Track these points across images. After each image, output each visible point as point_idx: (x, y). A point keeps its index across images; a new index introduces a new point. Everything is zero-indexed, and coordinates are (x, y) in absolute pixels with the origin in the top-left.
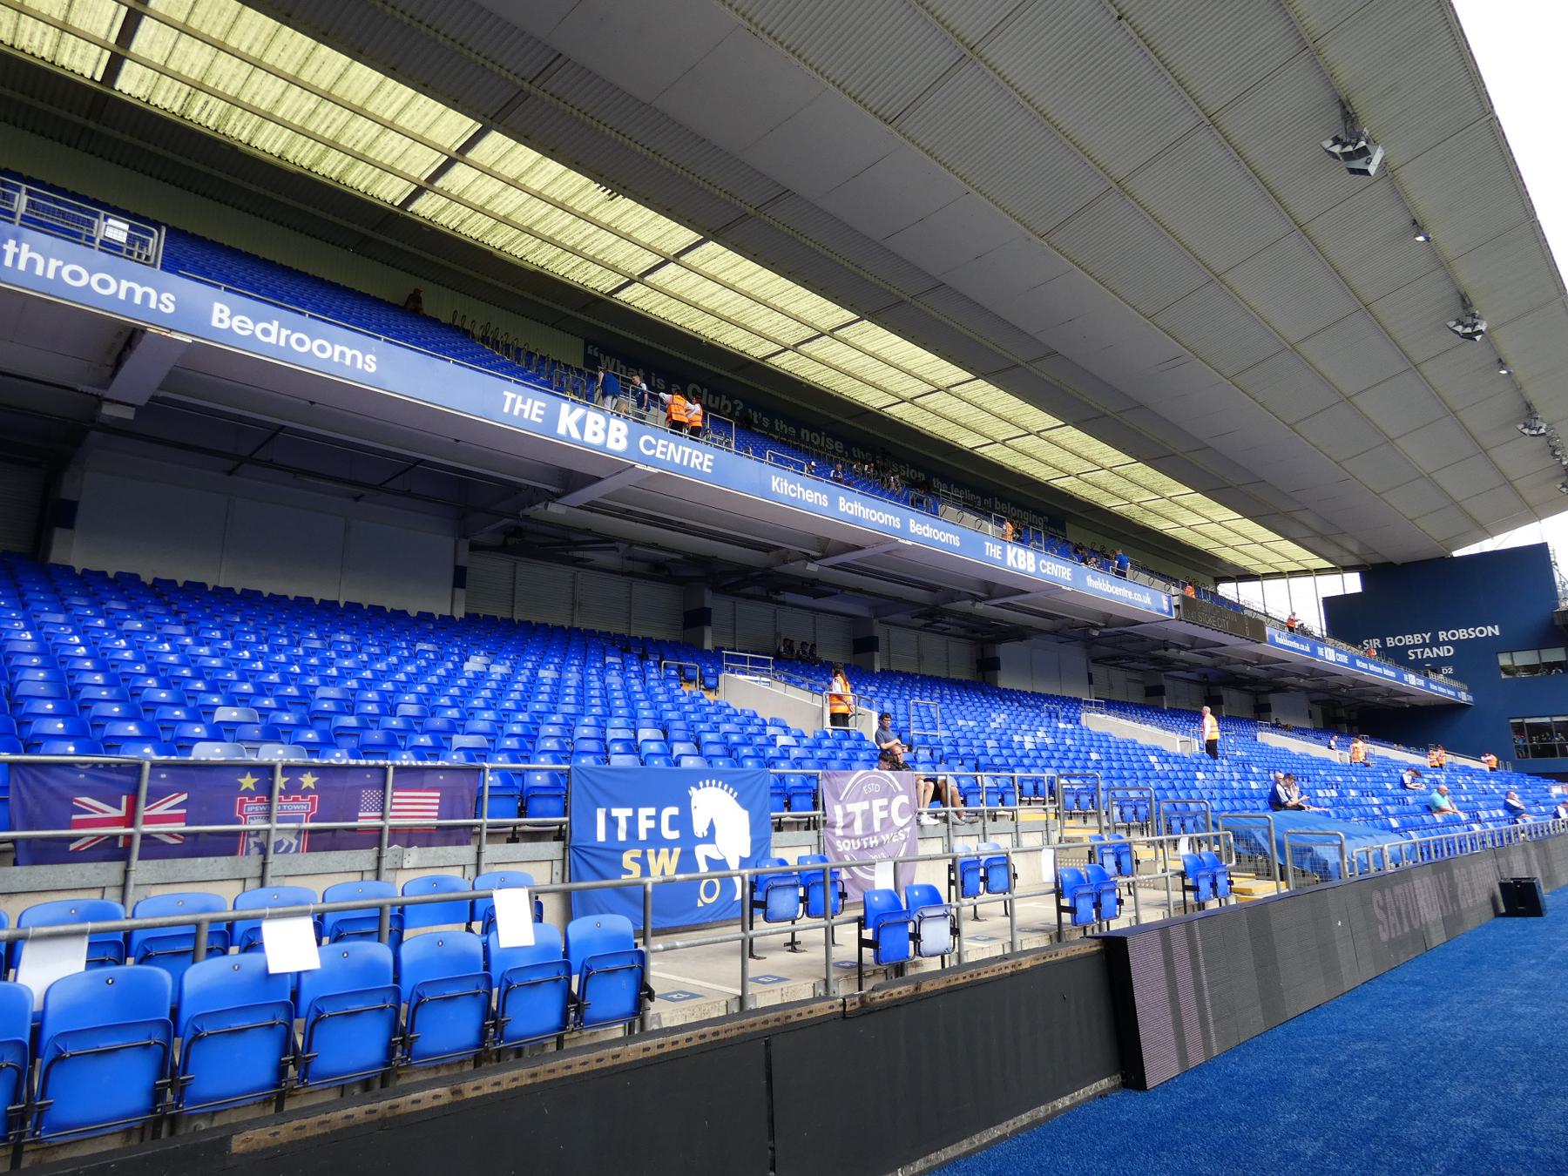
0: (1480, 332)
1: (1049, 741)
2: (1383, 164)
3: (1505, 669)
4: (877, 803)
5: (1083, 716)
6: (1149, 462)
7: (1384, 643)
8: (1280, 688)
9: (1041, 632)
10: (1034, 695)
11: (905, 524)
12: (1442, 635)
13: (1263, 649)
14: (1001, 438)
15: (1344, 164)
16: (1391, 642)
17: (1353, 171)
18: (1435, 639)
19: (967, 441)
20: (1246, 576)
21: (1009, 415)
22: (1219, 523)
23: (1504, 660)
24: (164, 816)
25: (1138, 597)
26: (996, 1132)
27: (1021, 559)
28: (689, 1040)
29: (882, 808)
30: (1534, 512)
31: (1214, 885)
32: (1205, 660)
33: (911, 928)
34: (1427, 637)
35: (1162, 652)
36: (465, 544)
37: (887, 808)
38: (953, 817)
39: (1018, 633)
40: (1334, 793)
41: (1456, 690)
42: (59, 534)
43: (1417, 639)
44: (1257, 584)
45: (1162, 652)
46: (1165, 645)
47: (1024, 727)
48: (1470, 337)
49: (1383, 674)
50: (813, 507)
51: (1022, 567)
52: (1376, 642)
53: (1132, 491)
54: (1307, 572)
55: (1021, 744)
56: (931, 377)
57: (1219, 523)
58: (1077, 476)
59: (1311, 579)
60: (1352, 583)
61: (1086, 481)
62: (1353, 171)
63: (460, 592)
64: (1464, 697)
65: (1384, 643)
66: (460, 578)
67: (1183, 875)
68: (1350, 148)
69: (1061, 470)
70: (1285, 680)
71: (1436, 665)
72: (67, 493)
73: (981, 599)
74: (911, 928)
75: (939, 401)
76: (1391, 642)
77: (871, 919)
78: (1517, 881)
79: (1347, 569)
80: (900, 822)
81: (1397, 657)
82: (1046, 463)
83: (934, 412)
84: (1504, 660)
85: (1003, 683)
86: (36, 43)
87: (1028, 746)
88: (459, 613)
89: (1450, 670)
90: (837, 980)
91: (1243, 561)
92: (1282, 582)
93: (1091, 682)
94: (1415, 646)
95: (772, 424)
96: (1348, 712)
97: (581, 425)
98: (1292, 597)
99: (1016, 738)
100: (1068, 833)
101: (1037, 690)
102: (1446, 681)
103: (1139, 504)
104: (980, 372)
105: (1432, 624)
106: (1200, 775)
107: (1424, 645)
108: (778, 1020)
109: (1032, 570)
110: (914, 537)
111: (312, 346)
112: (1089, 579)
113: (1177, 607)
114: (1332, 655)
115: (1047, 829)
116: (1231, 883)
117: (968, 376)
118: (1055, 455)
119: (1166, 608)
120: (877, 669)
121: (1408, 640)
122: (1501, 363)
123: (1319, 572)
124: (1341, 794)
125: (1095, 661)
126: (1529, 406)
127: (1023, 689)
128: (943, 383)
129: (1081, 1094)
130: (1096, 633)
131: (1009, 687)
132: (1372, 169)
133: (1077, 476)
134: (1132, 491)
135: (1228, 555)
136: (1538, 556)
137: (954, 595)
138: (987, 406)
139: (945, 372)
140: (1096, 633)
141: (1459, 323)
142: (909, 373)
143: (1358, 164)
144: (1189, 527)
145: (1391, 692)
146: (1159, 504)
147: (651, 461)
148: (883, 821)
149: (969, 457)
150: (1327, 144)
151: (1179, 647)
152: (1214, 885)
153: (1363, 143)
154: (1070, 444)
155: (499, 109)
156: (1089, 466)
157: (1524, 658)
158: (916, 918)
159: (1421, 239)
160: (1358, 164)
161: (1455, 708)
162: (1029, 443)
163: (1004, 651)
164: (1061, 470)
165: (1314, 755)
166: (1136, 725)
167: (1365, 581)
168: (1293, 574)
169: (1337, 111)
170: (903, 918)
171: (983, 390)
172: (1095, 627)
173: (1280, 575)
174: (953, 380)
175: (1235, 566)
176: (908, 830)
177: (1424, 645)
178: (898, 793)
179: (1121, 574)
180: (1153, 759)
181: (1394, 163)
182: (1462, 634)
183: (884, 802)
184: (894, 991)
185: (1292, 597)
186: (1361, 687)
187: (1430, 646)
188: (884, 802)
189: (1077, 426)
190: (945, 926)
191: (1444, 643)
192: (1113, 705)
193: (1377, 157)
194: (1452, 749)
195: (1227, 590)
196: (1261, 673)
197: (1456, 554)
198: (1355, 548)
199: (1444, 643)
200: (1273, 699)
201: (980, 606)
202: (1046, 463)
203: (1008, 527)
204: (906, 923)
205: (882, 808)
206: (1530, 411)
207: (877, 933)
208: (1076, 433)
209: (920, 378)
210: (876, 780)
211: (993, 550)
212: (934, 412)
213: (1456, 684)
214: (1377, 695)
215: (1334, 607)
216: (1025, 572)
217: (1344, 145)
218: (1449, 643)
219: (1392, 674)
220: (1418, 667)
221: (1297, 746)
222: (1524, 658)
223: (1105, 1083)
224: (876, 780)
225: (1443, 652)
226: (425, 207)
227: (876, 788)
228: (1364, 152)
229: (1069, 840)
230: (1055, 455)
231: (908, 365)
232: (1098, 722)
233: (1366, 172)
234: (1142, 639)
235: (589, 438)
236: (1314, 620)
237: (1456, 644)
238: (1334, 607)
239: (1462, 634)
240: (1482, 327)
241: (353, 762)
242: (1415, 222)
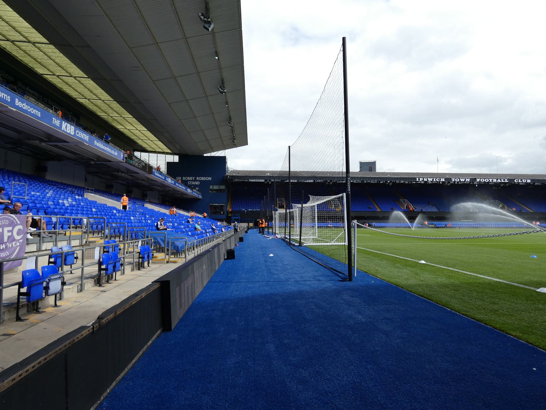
0: (225, 92)
1: (74, 203)
2: (213, 30)
3: (211, 190)
4: (6, 229)
5: (85, 194)
6: (119, 102)
7: (182, 178)
8: (151, 189)
9: (69, 159)
10: (62, 184)
11: (13, 101)
12: (198, 178)
13: (151, 176)
14: (57, 74)
15: (203, 23)
16: (184, 178)
17: (205, 27)
18: (195, 179)
19: (40, 70)
20: (144, 150)
21: (63, 65)
22: (139, 131)
23: (211, 187)
25: (113, 152)
26: (134, 361)
27: (68, 128)
28: (33, 367)
29: (9, 231)
30: (225, 148)
31: (148, 256)
32: (130, 177)
33: (45, 284)
35: (116, 173)
37: (11, 231)
38: (43, 235)
39: (58, 158)
40: (171, 224)
41: (199, 195)
43: (191, 178)
44: (147, 154)
45: (116, 173)
46: (118, 171)
47: (62, 197)
48: (222, 93)
49: (181, 188)
51: (68, 132)
52: (180, 178)
53: (110, 111)
54: (163, 153)
55: (64, 205)
56: (26, 35)
57: (139, 131)
58: (89, 100)
60: (176, 159)
61: (92, 103)
62: (205, 27)
64: (200, 197)
65: (182, 178)
67: (139, 253)
68: (206, 19)
69: (83, 95)
70: (154, 187)
71: (195, 186)
73: (44, 141)
74: (45, 284)
75: (28, 47)
76: (184, 178)
77: (25, 283)
78: (231, 250)
80: (17, 237)
81: (185, 183)
82: (76, 91)
83: (24, 51)
84: (211, 187)
85: (48, 177)
87: (67, 205)
89: (197, 189)
90: (4, 313)
91: (144, 145)
93: (86, 181)
94: (190, 181)
96: (170, 199)
98: (159, 160)
99: (60, 201)
100: (91, 240)
101: (63, 182)
102: (197, 192)
103: (111, 117)
104: (52, 41)
106: (132, 218)
107: (192, 181)
108: (70, 343)
109: (73, 133)
110: (17, 107)
112: (95, 142)
113: (126, 158)
114: (170, 181)
115: (81, 238)
116: (153, 255)
117: (48, 42)
118: (81, 88)
119: (122, 158)
121: (189, 178)
122: (227, 103)
123: (167, 153)
124: (173, 225)
125: (89, 173)
126: (230, 117)
127: (57, 180)
128: (32, 40)
129: (154, 338)
130: (93, 163)
131: (51, 179)
132: (210, 29)
133: (89, 100)
134: (110, 111)
135: (140, 142)
136: (223, 160)
137: (31, 137)
138: (53, 58)
139: (34, 35)
140: (93, 163)
141: (220, 88)
142: (14, 28)
143: (207, 26)
144: (128, 130)
145: (183, 194)
146: (119, 119)
148: (9, 237)
149: (40, 78)
150: (200, 14)
151: (122, 172)
152: (148, 256)
153: (210, 20)
154: (88, 86)
156: (94, 97)
157: (216, 187)
158: (47, 280)
159: (217, 58)
160: (207, 26)
161: (197, 200)
162: (70, 80)
163: (50, 164)
164: (83, 95)
165: (161, 211)
166: (107, 199)
168: (159, 153)
169: (204, 5)
170: (41, 281)
171: (51, 49)
172: (93, 160)
173: (155, 152)
174: (38, 40)
175: (141, 146)
176: (21, 241)
177: (192, 181)
178: (17, 224)
179: (107, 142)
180: (115, 212)
181: (215, 31)
182: (202, 179)
183: (10, 228)
184: (109, 317)
185: (159, 160)
186: (175, 191)
188: (10, 228)
189: (93, 80)
190: (59, 282)
191: (198, 181)
192: (97, 191)
193: (212, 26)
194: (197, 212)
195: (137, 154)
196: (147, 184)
197: (205, 155)
198: (178, 148)
199: (198, 181)
200: (149, 193)
201: (43, 144)
202: (76, 91)
203: (60, 113)
204: (42, 283)
205: (9, 231)
206: (230, 119)
207: (29, 289)
208: (92, 82)
209: (20, 33)
210: (6, 219)
211: (56, 122)
212: (24, 51)
213: (199, 193)
214: (178, 194)
216: (70, 134)
217: (205, 18)
218: (199, 181)
219: (184, 188)
220: (190, 187)
221: (156, 208)
222: (216, 187)
223: (159, 332)
224: (6, 219)
225: (197, 183)
227: (7, 222)
228: (209, 23)
229: (90, 242)
230: (81, 88)
231: (14, 24)
232: (91, 197)
233: (208, 30)
234: (109, 167)
236: (164, 169)
237: (201, 181)
239: (202, 179)
240: (225, 91)
241: (180, 261)
242: (216, 52)
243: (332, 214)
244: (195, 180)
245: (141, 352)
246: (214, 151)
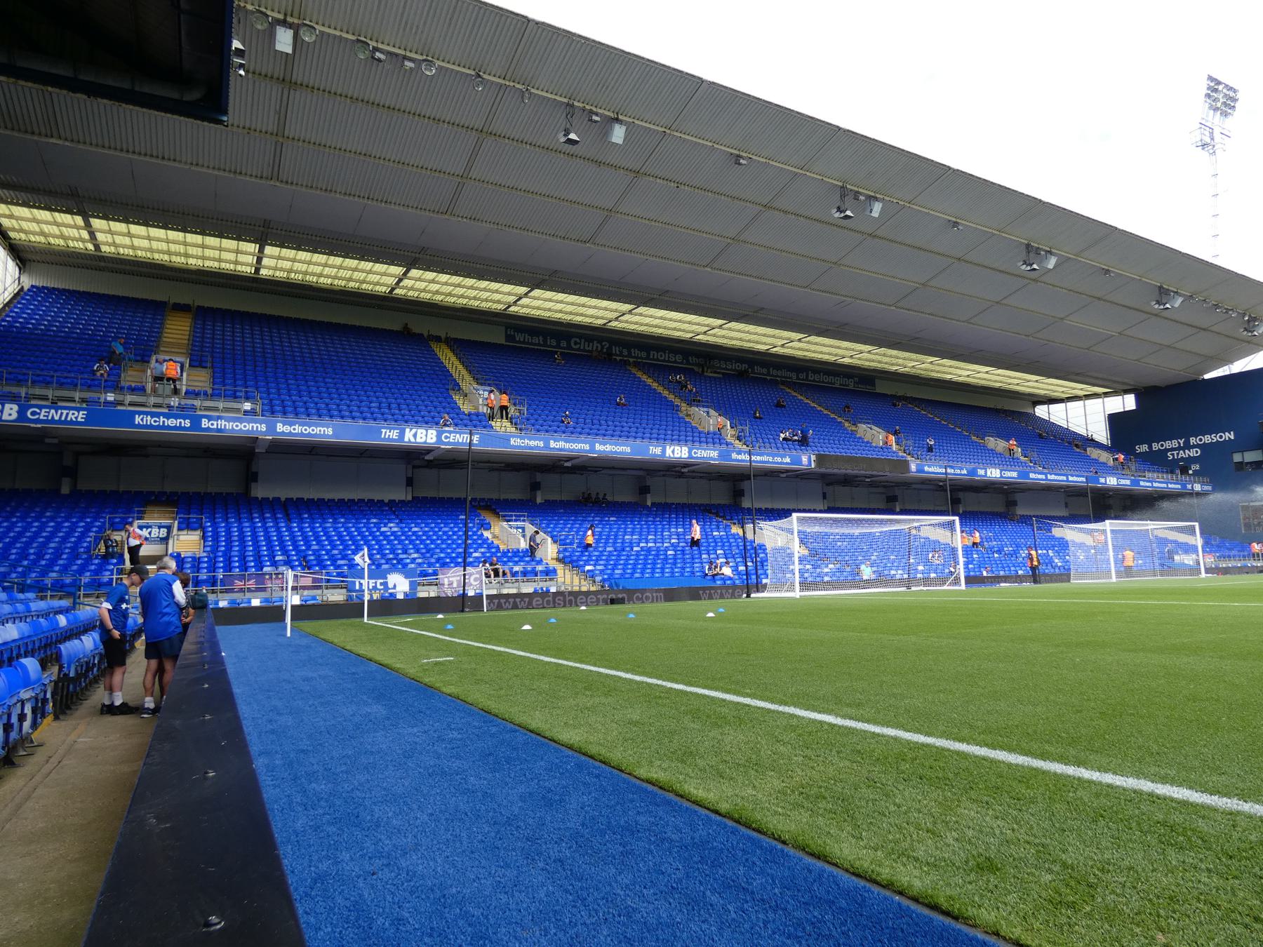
12: (1193, 441)
24: (251, 584)
34: (1181, 442)
36: (410, 467)
42: (253, 485)
43: (1175, 443)
50: (537, 447)
59: (1100, 400)
60: (1129, 402)
63: (410, 489)
66: (410, 482)
72: (254, 469)
79: (1126, 392)
84: (1237, 458)
85: (746, 504)
86: (263, 85)
88: (410, 498)
89: (1196, 467)
92: (1080, 403)
93: (824, 497)
94: (1173, 449)
95: (630, 353)
97: (415, 436)
105: (1185, 433)
107: (1179, 448)
111: (309, 430)
120: (649, 503)
122: (1107, 271)
125: (828, 485)
147: (449, 443)
155: (410, 264)
167: (1138, 401)
177: (1179, 448)
182: (1207, 439)
187: (1183, 449)
191: (1194, 446)
197: (1207, 376)
199: (1194, 446)
215: (1115, 421)
218: (1197, 446)
225: (1193, 453)
226: (399, 292)
235: (419, 440)
236: (1101, 433)
237: (1203, 447)
238: (1115, 421)
239: (1207, 439)
243: (697, 583)
244: (1188, 446)
245: (502, 649)
246: (1230, 361)
